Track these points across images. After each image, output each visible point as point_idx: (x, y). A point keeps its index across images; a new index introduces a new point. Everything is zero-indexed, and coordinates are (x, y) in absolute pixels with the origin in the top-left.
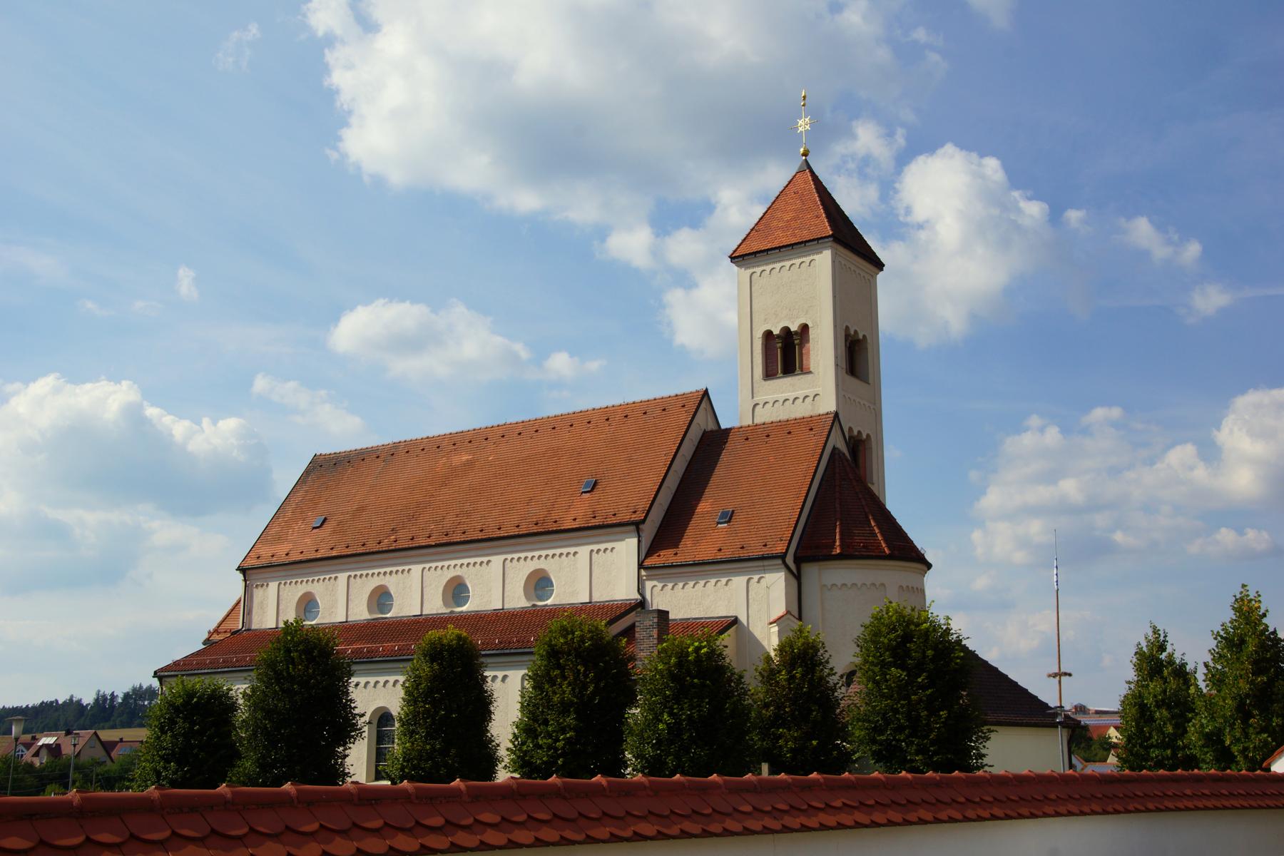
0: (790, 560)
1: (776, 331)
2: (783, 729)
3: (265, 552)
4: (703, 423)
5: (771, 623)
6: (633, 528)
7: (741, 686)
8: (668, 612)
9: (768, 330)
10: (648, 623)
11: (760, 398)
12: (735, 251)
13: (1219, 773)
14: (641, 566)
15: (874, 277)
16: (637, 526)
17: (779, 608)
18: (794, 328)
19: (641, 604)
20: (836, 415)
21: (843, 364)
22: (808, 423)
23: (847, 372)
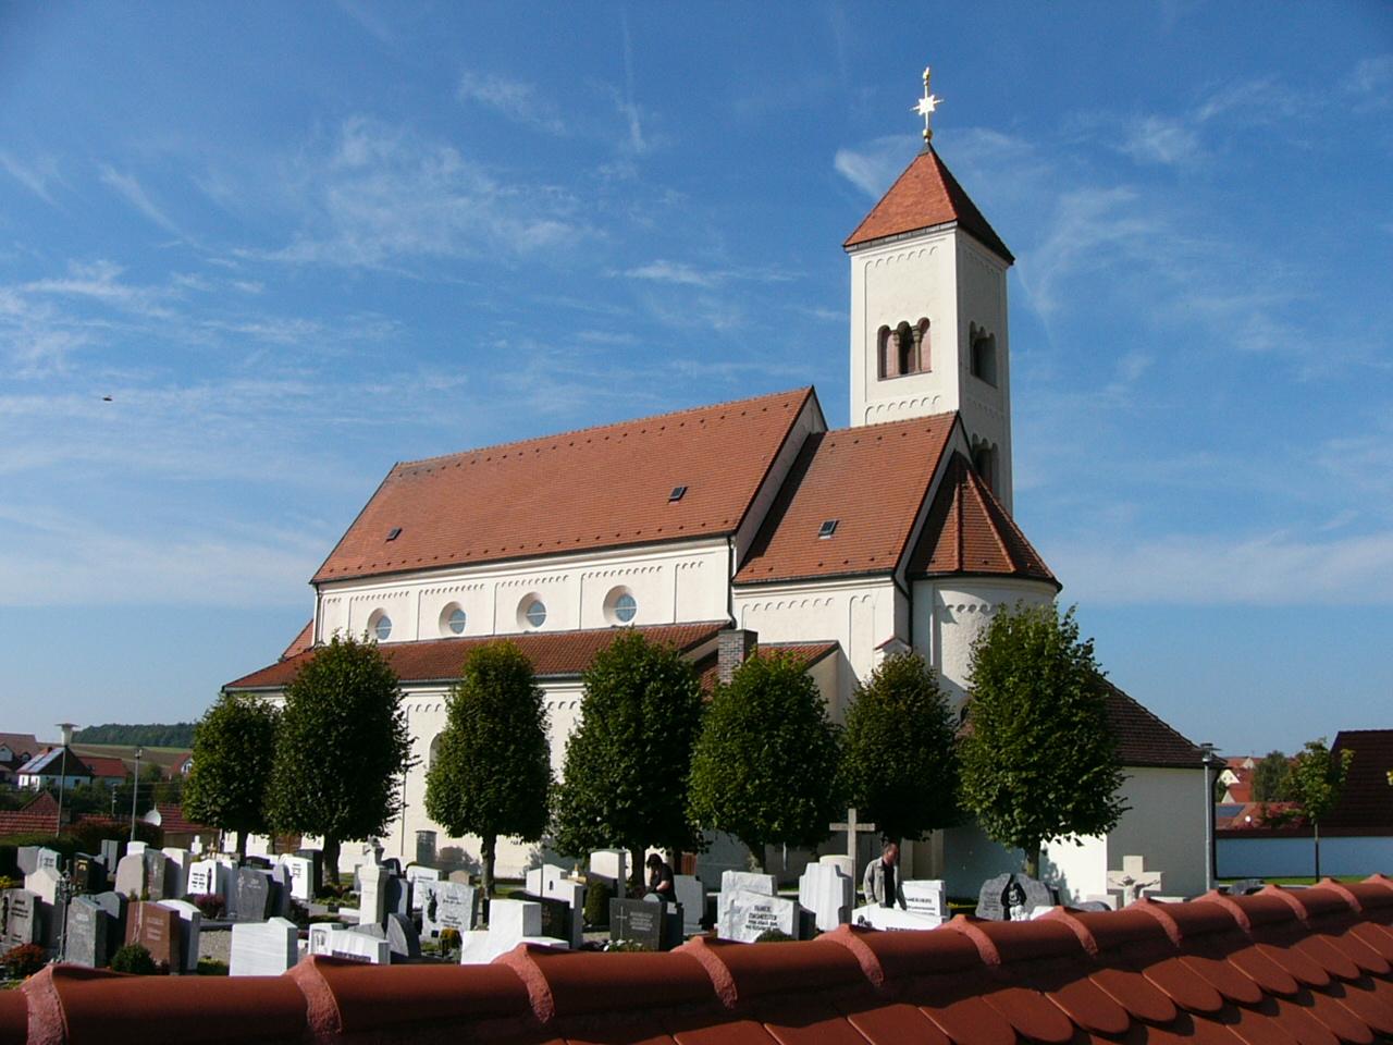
0: (900, 575)
1: (894, 327)
2: (665, 738)
3: (338, 565)
4: (807, 424)
5: (877, 649)
6: (724, 540)
7: (948, 749)
8: (756, 634)
9: (882, 327)
10: (732, 645)
11: (875, 402)
12: (849, 239)
13: (268, 699)
14: (732, 582)
15: (1003, 270)
16: (728, 536)
17: (887, 631)
18: (913, 323)
19: (731, 625)
20: (958, 413)
21: (968, 363)
22: (927, 424)
23: (971, 373)
